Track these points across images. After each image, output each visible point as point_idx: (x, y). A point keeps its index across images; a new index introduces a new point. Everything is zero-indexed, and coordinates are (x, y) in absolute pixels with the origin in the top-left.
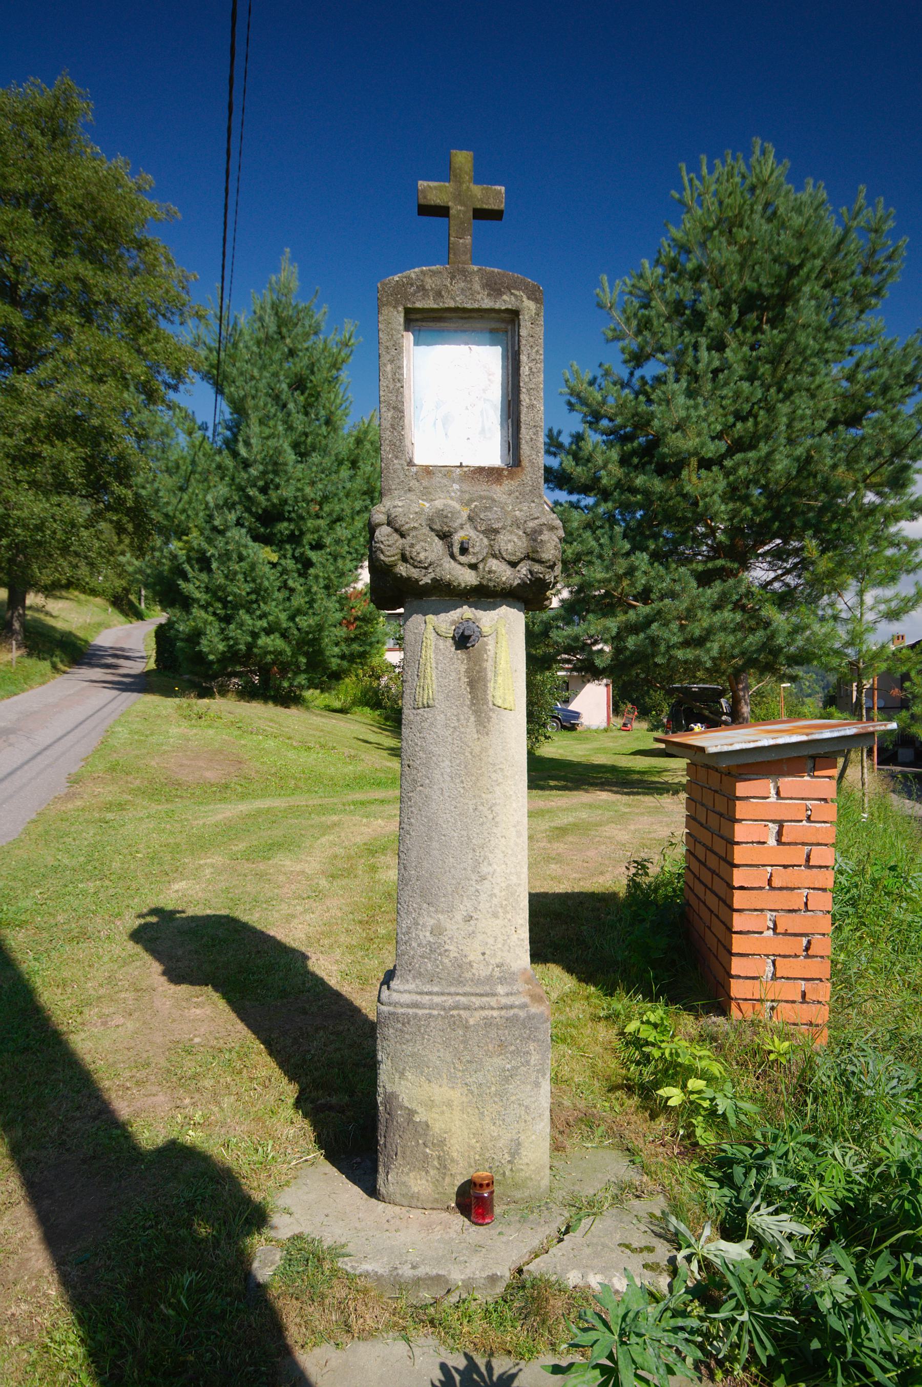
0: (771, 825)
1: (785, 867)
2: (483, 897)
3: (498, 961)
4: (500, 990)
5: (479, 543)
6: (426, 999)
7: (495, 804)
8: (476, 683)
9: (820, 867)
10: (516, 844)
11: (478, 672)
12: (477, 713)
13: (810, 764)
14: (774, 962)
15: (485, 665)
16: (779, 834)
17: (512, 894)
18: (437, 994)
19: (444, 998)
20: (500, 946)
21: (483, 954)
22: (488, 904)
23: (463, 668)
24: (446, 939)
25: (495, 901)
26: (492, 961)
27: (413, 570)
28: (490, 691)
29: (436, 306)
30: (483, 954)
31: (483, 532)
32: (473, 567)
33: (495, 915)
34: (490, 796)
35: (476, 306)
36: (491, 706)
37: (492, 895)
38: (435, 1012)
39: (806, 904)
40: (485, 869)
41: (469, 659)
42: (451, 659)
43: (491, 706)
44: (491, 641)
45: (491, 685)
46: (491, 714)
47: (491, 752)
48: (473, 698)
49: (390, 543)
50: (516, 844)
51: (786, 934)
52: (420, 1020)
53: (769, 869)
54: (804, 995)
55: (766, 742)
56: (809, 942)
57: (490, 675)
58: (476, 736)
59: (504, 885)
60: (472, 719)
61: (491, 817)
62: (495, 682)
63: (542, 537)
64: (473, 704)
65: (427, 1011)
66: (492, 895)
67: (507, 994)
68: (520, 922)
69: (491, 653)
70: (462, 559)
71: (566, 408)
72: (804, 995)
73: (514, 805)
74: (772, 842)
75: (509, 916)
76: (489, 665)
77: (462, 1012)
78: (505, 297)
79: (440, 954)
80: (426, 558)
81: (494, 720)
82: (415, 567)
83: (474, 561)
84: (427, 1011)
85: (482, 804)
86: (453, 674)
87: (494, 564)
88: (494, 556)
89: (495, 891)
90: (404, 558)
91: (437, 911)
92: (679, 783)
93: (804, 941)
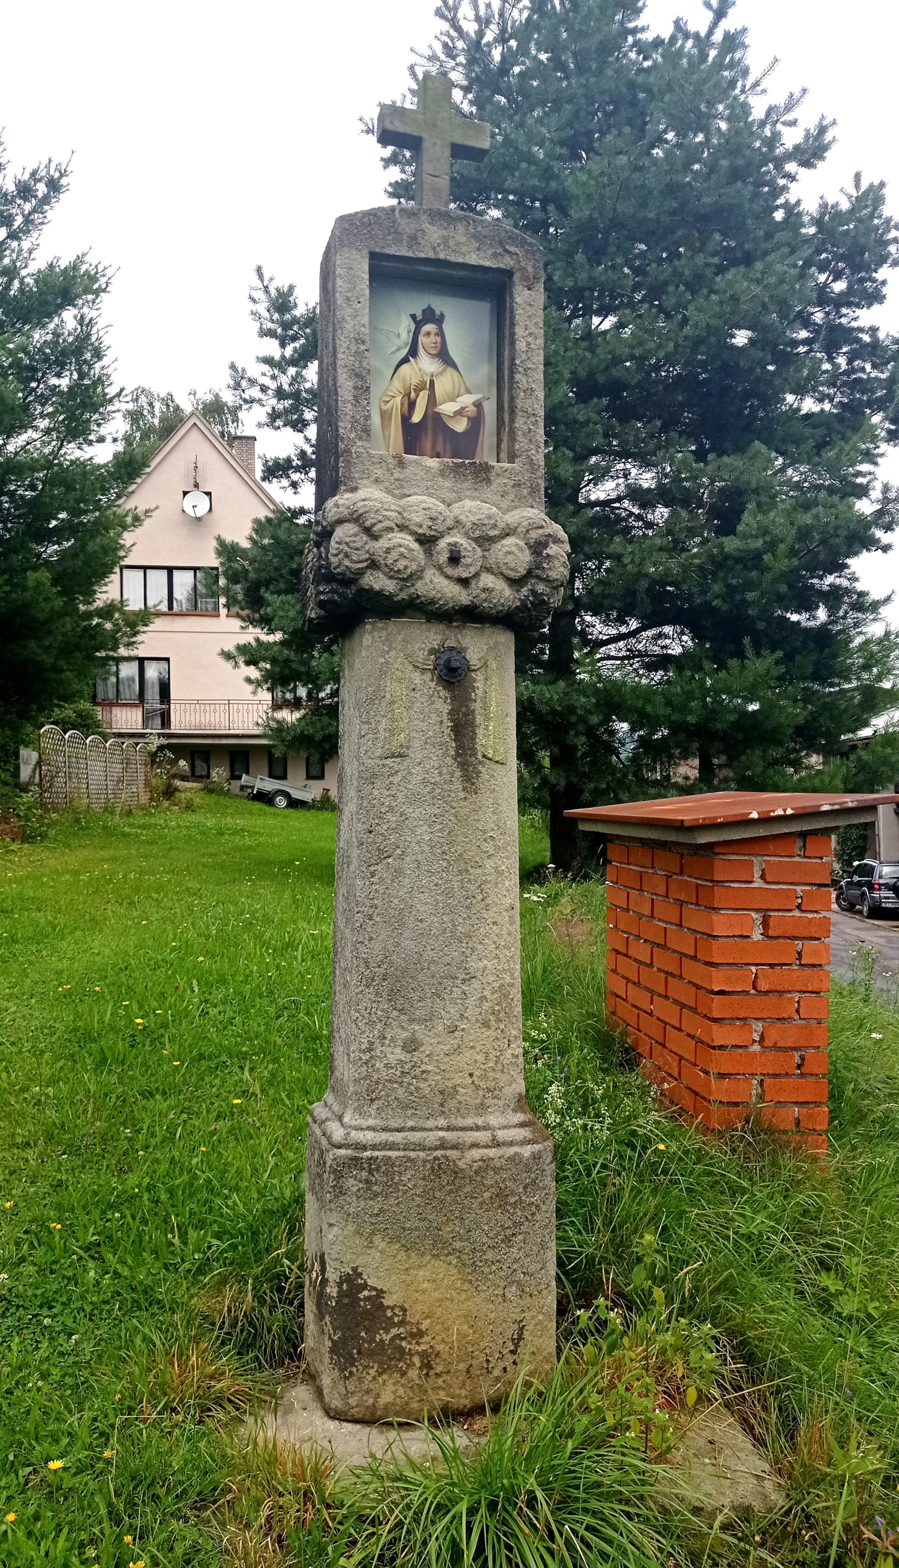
0: (754, 915)
1: (772, 966)
2: (472, 1001)
5: (471, 552)
6: (398, 1137)
8: (462, 728)
9: (813, 966)
10: (509, 934)
11: (466, 715)
12: (464, 766)
13: (799, 843)
14: (761, 1083)
15: (473, 706)
16: (765, 924)
17: (506, 996)
18: (412, 1129)
19: (424, 1134)
21: (471, 1075)
22: (478, 1010)
23: (446, 708)
24: (422, 1056)
25: (486, 1006)
27: (388, 582)
28: (481, 740)
29: (410, 254)
30: (471, 1075)
31: (476, 540)
32: (464, 582)
34: (479, 871)
35: (461, 260)
36: (480, 757)
38: (412, 1154)
39: (797, 1011)
40: (474, 965)
41: (453, 698)
42: (431, 696)
43: (480, 757)
44: (479, 677)
45: (480, 732)
48: (458, 748)
49: (358, 545)
50: (509, 934)
51: (775, 1047)
52: (393, 1165)
53: (753, 969)
54: (798, 1123)
56: (802, 1058)
57: (479, 719)
58: (462, 795)
59: (496, 985)
60: (458, 774)
61: (479, 897)
62: (487, 728)
63: (548, 551)
64: (458, 755)
65: (401, 1153)
66: (483, 998)
68: (514, 1033)
69: (479, 692)
70: (449, 571)
72: (798, 1123)
73: (507, 883)
74: (757, 936)
76: (477, 706)
77: (449, 1153)
79: (415, 1077)
80: (406, 567)
81: (485, 776)
82: (391, 578)
83: (465, 575)
84: (401, 1153)
85: (469, 881)
86: (433, 716)
87: (487, 580)
88: (489, 570)
90: (374, 565)
91: (412, 1021)
93: (797, 1056)
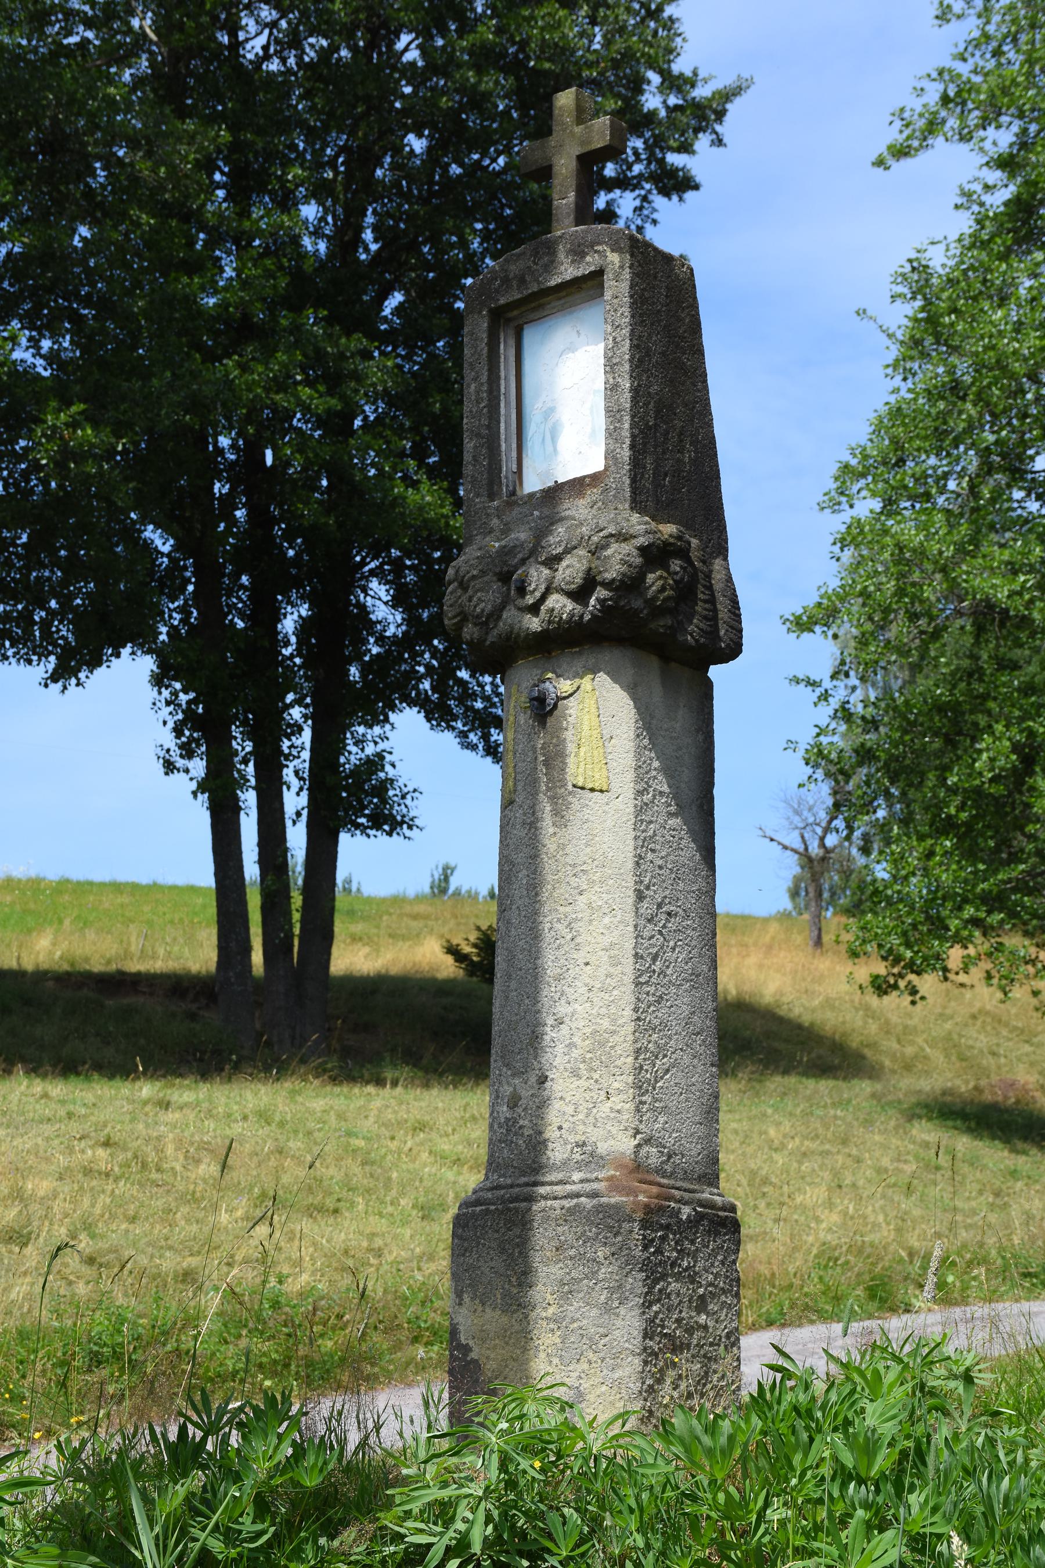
3: (580, 1138)
4: (576, 1176)
7: (576, 920)
20: (581, 1116)
25: (575, 1053)
26: (572, 1139)
33: (576, 1074)
34: (569, 909)
37: (571, 1045)
43: (570, 788)
46: (570, 799)
47: (569, 849)
55: (260, 931)
66: (571, 1045)
67: (582, 1181)
71: (159, 767)
75: (596, 1076)
78: (588, 259)
85: (559, 920)
89: (575, 1039)
92: (129, 944)
